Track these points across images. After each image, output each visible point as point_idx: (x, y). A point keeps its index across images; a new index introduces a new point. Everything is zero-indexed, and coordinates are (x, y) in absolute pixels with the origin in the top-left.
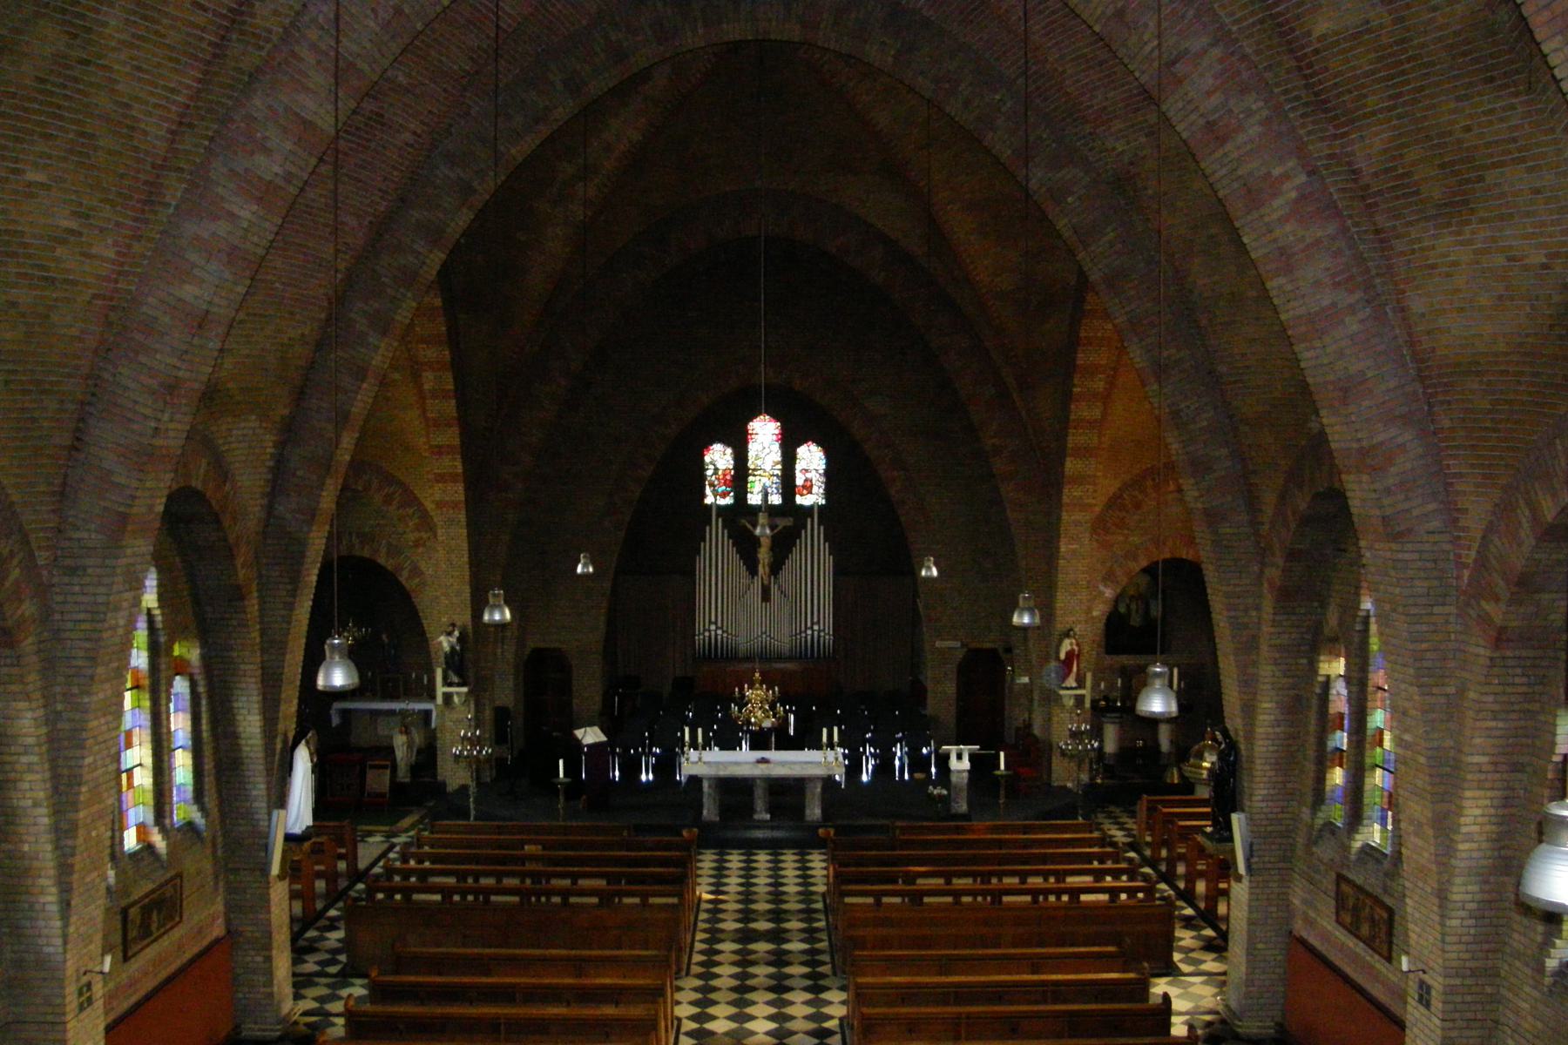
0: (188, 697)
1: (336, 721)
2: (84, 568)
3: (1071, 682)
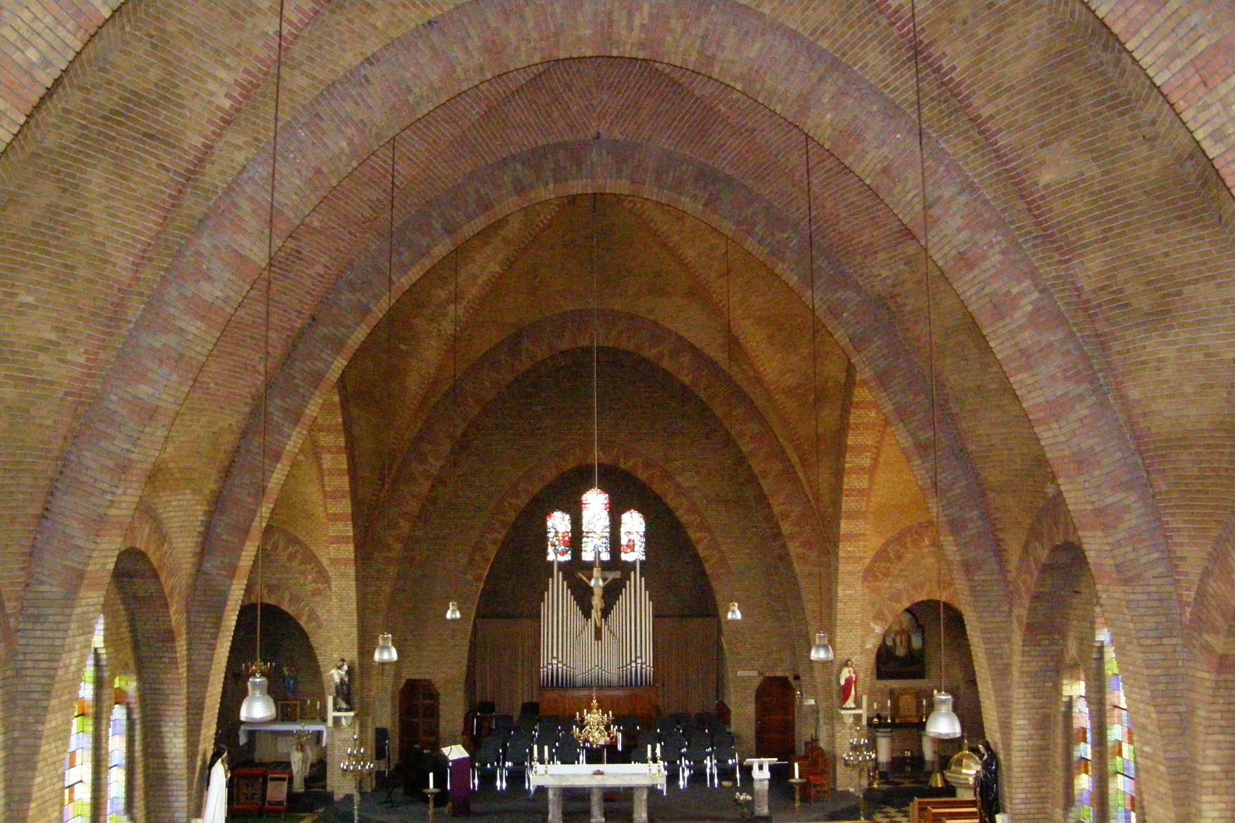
0: (124, 722)
1: (243, 740)
2: (46, 616)
3: (850, 703)
